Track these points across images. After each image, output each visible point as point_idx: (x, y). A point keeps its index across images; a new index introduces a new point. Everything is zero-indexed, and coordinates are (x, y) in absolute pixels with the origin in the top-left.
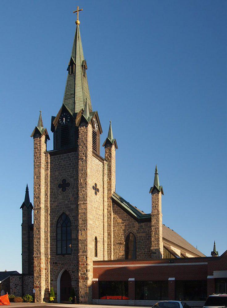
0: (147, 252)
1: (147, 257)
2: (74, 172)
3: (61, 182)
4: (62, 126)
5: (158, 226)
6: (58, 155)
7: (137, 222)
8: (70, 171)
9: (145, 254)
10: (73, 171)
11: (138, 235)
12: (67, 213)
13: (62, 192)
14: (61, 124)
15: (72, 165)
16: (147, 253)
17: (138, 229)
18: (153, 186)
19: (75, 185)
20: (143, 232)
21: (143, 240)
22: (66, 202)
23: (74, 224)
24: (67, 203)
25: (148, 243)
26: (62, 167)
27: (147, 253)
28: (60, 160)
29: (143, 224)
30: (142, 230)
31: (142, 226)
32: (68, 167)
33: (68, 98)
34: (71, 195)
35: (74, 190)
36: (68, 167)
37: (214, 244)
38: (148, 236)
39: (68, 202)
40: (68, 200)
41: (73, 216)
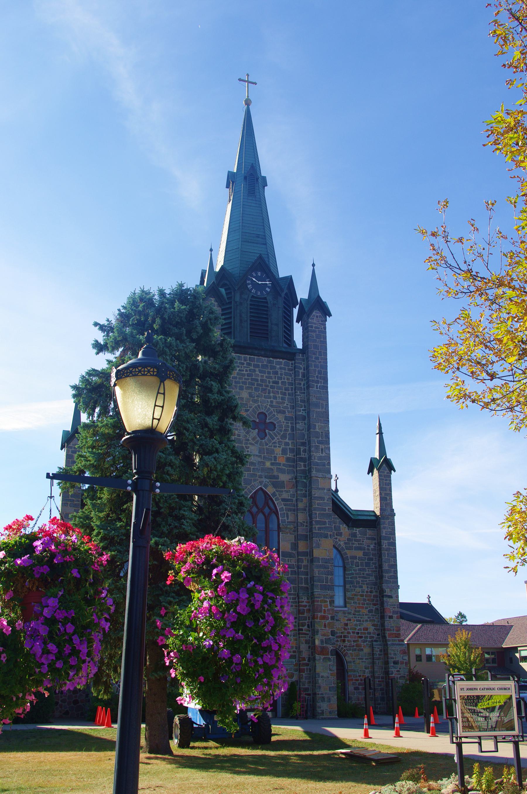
0: (367, 592)
1: (367, 604)
2: (286, 402)
3: (271, 421)
4: (253, 297)
5: (393, 540)
6: (248, 355)
7: (345, 525)
8: (275, 398)
9: (362, 596)
10: (283, 399)
11: (349, 553)
12: (270, 490)
13: (258, 438)
14: (251, 292)
15: (280, 385)
16: (366, 596)
17: (348, 539)
18: (69, 428)
19: (288, 430)
20: (357, 548)
21: (358, 566)
22: (268, 464)
23: (286, 518)
24: (270, 467)
25: (367, 572)
26: (258, 385)
27: (366, 596)
28: (252, 368)
29: (357, 530)
30: (356, 544)
31: (354, 535)
32: (272, 387)
33: (249, 241)
34: (278, 451)
35: (287, 440)
36: (272, 387)
37: (39, 515)
38: (367, 557)
39: (272, 464)
40: (271, 460)
41: (283, 500)
